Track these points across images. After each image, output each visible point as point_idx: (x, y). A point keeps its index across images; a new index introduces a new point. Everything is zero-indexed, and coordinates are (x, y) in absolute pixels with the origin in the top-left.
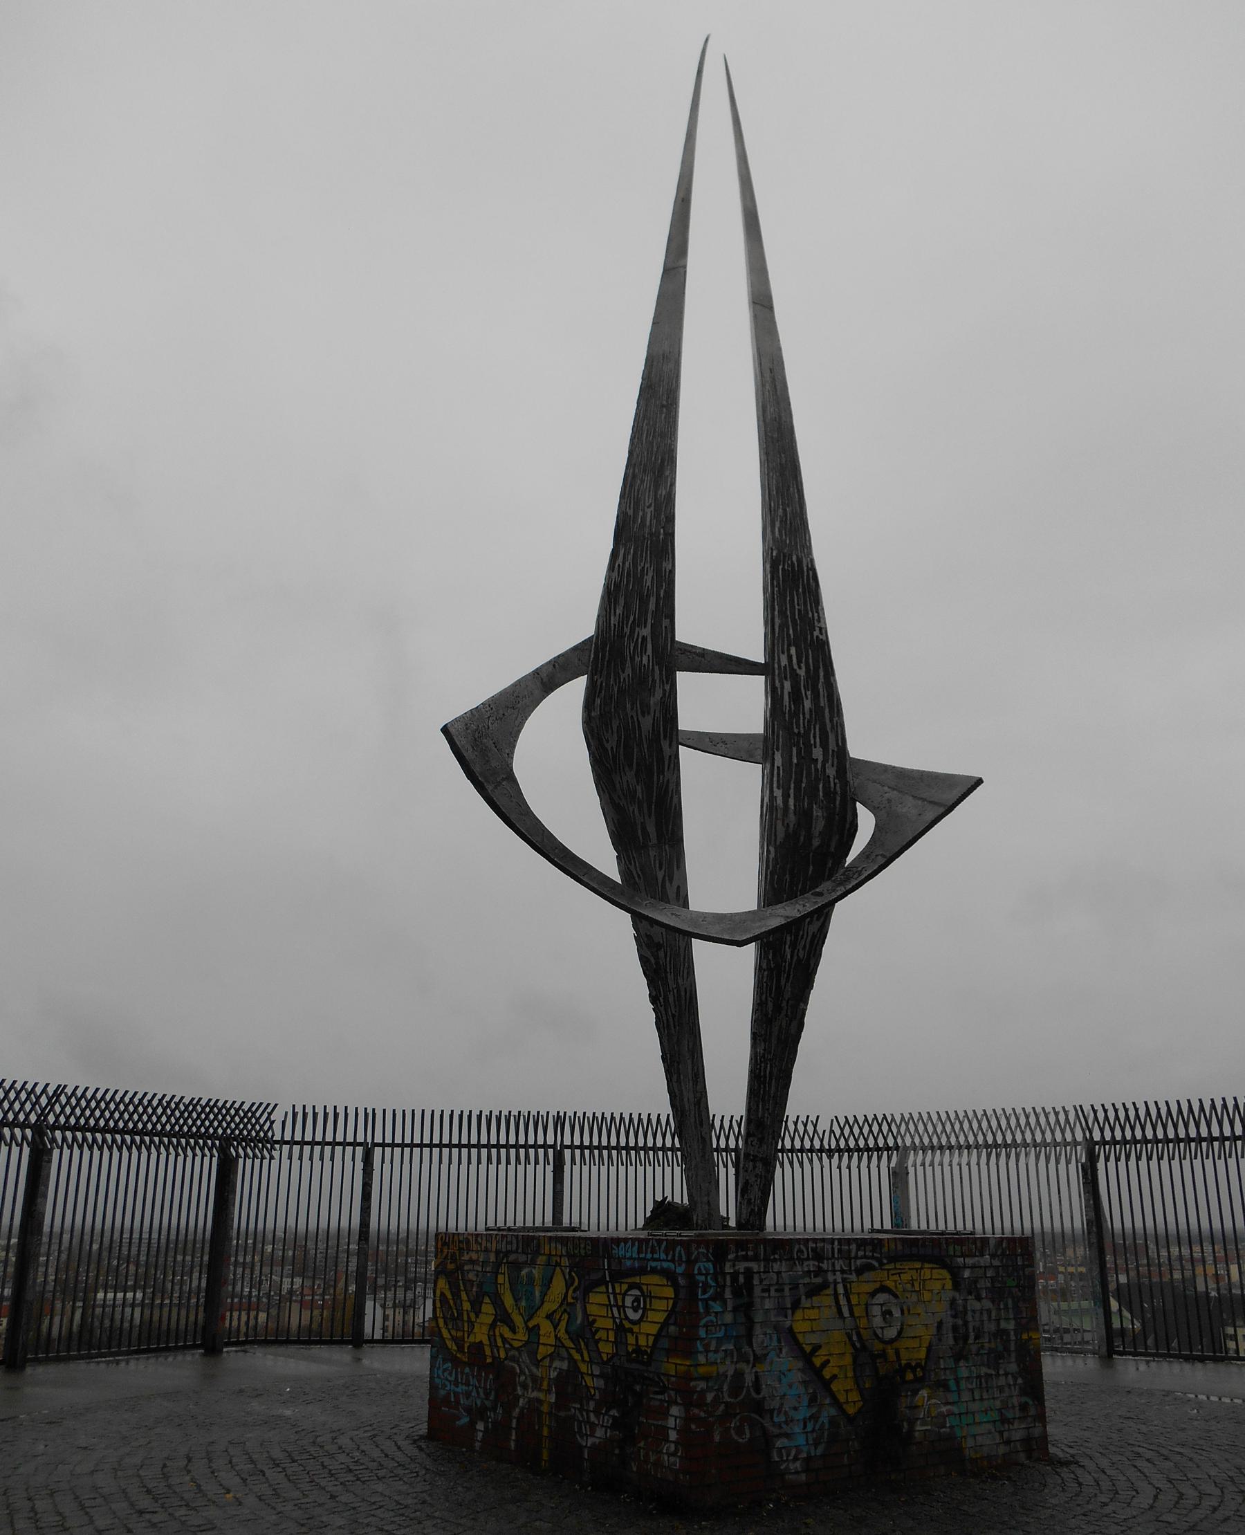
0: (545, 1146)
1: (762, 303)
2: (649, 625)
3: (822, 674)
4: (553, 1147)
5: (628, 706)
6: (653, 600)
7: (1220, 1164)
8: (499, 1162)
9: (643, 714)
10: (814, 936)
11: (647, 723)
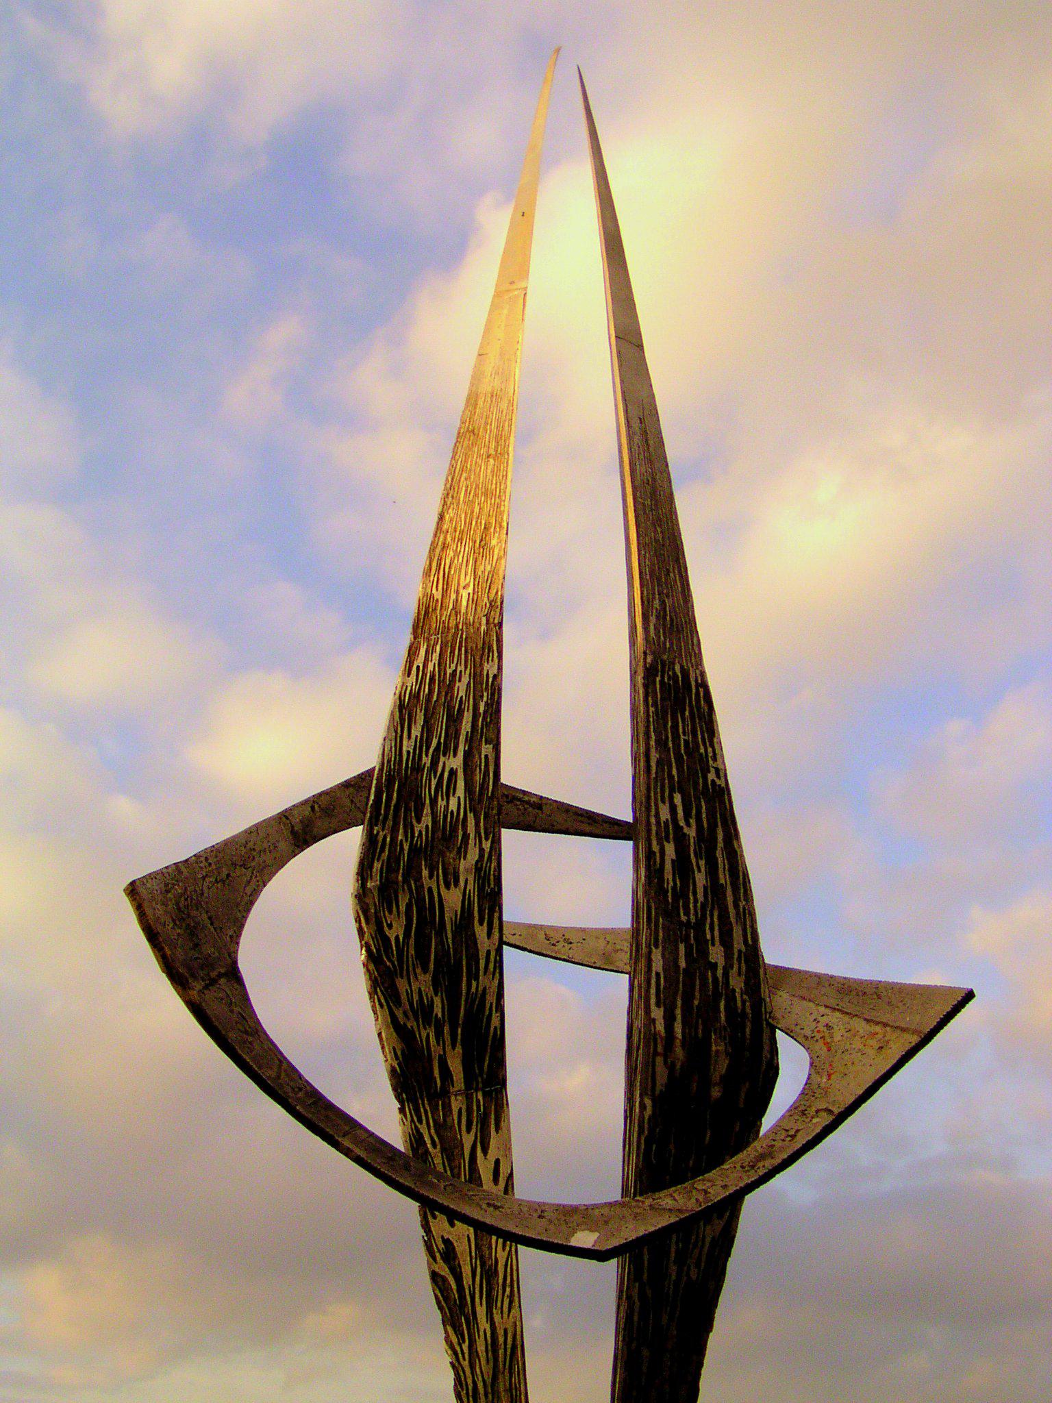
2: (461, 754)
3: (720, 836)
5: (425, 873)
6: (467, 717)
9: (448, 886)
10: (714, 1242)
11: (453, 899)
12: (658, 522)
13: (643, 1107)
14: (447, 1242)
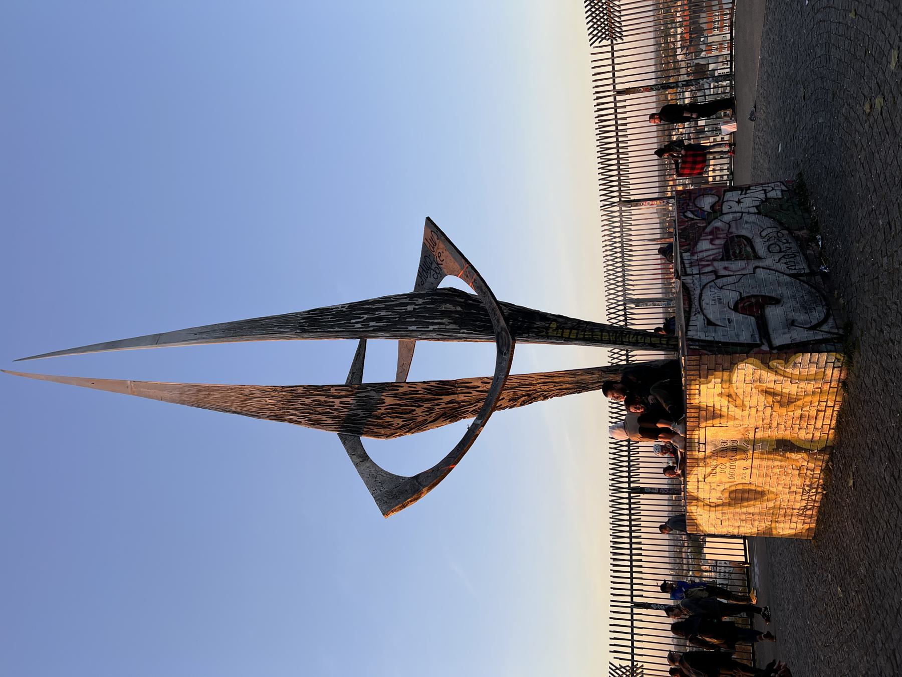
0: (630, 498)
1: (157, 339)
4: (629, 493)
6: (319, 398)
7: (632, 187)
8: (640, 549)
12: (241, 328)
13: (463, 333)
14: (510, 400)
